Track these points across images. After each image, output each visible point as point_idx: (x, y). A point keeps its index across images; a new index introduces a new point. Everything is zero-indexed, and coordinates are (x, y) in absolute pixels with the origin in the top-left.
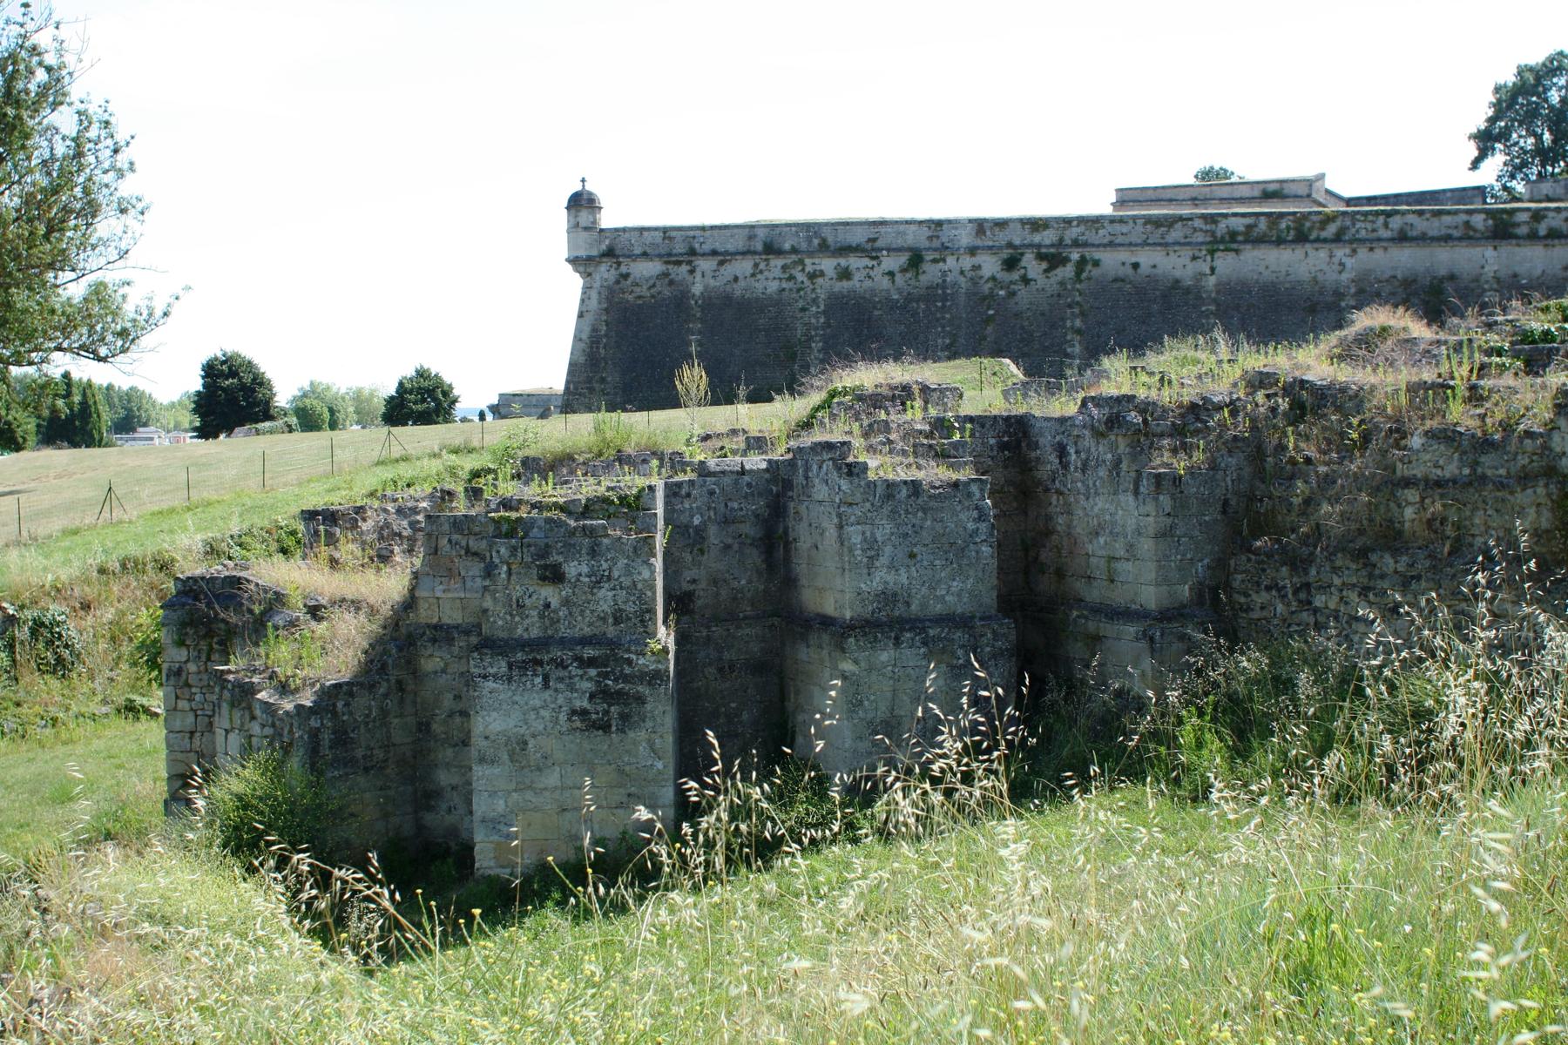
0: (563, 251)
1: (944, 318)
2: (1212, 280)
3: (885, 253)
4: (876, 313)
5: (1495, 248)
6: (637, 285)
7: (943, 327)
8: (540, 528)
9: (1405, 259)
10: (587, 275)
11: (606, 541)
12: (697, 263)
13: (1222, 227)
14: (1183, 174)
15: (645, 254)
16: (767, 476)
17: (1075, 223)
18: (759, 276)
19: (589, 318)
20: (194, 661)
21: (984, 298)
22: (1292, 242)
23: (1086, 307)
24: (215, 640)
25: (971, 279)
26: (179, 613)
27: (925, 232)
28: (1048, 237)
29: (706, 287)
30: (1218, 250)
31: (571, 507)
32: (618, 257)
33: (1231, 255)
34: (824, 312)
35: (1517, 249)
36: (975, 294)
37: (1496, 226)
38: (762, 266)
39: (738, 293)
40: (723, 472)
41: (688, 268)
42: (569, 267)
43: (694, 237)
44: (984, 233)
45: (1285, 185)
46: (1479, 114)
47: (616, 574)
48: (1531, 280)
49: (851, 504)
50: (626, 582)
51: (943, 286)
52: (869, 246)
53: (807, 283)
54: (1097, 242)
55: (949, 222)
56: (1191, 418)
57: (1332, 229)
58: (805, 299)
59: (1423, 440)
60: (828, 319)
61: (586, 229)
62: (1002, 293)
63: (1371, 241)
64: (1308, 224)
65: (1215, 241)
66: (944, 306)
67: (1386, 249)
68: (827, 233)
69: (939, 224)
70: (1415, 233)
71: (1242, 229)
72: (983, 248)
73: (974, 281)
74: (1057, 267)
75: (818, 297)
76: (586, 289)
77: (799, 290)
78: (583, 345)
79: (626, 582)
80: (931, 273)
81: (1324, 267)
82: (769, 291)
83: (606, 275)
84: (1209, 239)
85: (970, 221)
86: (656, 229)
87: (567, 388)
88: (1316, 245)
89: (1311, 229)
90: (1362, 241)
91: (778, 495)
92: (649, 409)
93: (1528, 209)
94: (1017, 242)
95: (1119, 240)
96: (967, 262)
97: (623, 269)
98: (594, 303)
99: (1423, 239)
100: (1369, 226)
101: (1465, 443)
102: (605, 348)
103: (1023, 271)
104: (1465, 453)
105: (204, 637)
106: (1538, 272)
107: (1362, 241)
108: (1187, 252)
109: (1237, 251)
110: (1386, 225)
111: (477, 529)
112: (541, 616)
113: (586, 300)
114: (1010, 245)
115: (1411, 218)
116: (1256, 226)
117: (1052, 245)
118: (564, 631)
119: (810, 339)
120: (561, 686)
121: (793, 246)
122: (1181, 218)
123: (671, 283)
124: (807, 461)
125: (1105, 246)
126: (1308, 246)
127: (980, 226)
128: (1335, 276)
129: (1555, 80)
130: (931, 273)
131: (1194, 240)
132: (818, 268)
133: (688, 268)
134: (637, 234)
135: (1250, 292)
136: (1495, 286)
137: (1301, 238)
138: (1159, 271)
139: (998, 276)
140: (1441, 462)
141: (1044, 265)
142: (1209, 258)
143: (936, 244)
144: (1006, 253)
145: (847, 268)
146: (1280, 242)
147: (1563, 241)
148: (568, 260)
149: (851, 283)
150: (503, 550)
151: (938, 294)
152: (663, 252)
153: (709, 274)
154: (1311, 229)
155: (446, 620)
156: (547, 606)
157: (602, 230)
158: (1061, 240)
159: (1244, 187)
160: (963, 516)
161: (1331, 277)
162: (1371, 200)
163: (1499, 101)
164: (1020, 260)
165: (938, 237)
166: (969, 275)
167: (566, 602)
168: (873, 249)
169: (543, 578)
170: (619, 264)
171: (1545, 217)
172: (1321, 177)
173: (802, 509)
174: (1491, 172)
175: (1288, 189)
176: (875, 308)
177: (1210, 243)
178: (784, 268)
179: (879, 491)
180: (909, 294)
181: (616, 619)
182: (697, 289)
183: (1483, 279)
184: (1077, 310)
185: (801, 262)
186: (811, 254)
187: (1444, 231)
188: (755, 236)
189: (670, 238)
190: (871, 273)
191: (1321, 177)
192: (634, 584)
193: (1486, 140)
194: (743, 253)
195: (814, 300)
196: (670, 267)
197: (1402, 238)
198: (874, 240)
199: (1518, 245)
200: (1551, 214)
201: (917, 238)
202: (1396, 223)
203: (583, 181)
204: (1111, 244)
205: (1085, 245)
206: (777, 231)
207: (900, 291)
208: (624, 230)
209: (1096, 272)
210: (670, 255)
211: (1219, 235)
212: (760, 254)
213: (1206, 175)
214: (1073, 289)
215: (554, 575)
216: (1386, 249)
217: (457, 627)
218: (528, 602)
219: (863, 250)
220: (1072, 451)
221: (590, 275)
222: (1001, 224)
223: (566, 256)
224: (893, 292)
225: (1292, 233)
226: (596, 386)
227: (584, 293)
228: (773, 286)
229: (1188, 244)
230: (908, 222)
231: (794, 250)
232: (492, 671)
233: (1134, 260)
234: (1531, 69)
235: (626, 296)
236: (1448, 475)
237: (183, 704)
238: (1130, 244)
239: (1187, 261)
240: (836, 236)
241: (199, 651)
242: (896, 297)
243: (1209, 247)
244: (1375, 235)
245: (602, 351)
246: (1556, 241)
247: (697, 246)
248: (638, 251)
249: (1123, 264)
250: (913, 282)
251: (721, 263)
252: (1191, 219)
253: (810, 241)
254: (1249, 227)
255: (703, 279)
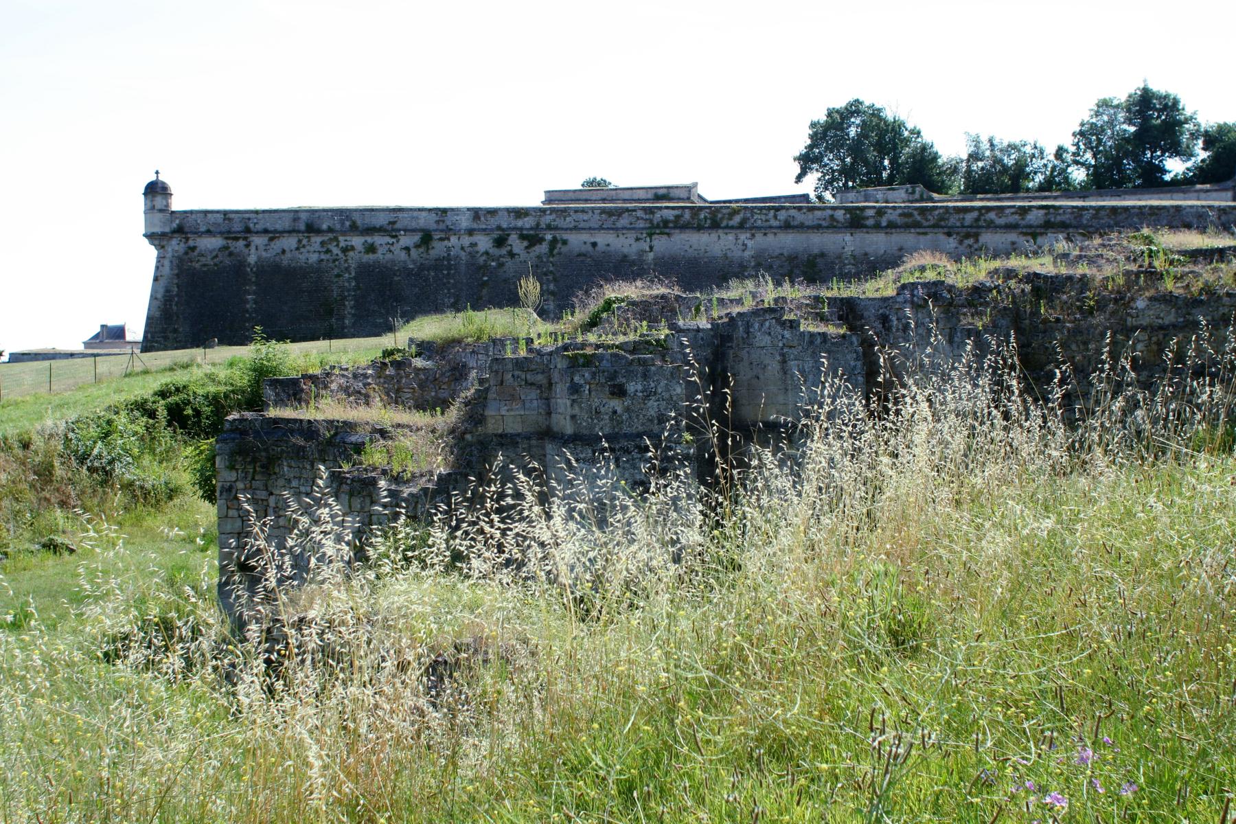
0: (142, 230)
1: (449, 283)
2: (651, 255)
3: (402, 232)
4: (396, 278)
5: (852, 234)
6: (203, 255)
7: (449, 290)
8: (607, 360)
9: (788, 242)
10: (160, 247)
11: (653, 368)
12: (251, 239)
13: (658, 216)
14: (575, 184)
15: (208, 232)
16: (712, 333)
17: (548, 212)
18: (302, 250)
19: (162, 282)
20: (242, 481)
21: (480, 268)
22: (709, 228)
23: (558, 275)
24: (258, 464)
25: (470, 253)
26: (231, 445)
27: (434, 217)
28: (528, 222)
29: (259, 258)
30: (655, 233)
31: (625, 347)
32: (187, 233)
33: (665, 237)
34: (355, 278)
35: (867, 236)
36: (472, 265)
37: (852, 218)
38: (305, 242)
39: (285, 263)
40: (688, 330)
41: (245, 243)
42: (146, 241)
43: (249, 219)
44: (479, 218)
45: (671, 190)
46: (801, 142)
47: (660, 390)
48: (877, 258)
49: (791, 347)
50: (666, 395)
51: (448, 258)
52: (389, 228)
53: (341, 255)
54: (565, 227)
55: (452, 210)
56: (976, 296)
57: (737, 219)
58: (339, 268)
59: (1147, 302)
60: (358, 283)
61: (161, 211)
62: (493, 264)
63: (765, 228)
64: (720, 216)
65: (653, 227)
66: (448, 274)
67: (775, 234)
68: (356, 217)
69: (444, 211)
70: (796, 223)
71: (672, 218)
72: (479, 230)
73: (472, 255)
74: (535, 245)
75: (349, 266)
76: (160, 259)
77: (334, 261)
78: (158, 303)
79: (666, 395)
80: (438, 248)
81: (732, 247)
82: (310, 261)
83: (176, 248)
84: (648, 225)
85: (469, 209)
86: (218, 212)
87: (145, 337)
88: (726, 231)
89: (722, 219)
90: (759, 228)
91: (718, 346)
92: (330, 338)
93: (874, 207)
94: (505, 226)
95: (582, 225)
96: (466, 241)
97: (191, 243)
98: (166, 270)
99: (801, 227)
100: (763, 217)
101: (1180, 302)
102: (176, 305)
103: (509, 248)
104: (1179, 308)
105: (250, 463)
106: (882, 252)
107: (759, 228)
108: (632, 235)
109: (668, 234)
110: (775, 217)
111: (533, 367)
112: (611, 419)
113: (161, 268)
114: (499, 228)
115: (793, 212)
116: (682, 216)
117: (531, 229)
118: (626, 429)
119: (344, 298)
120: (627, 465)
121: (329, 227)
122: (627, 210)
123: (231, 254)
124: (748, 322)
125: (571, 229)
126: (720, 231)
127: (476, 213)
128: (740, 253)
129: (853, 120)
130: (438, 248)
131: (637, 226)
132: (349, 244)
133: (245, 243)
134: (202, 215)
135: (679, 265)
136: (852, 261)
137: (715, 225)
138: (612, 248)
139: (491, 251)
140: (1162, 315)
141: (526, 243)
142: (648, 239)
143: (442, 226)
144: (496, 234)
145: (373, 244)
146: (699, 228)
147: (898, 230)
148: (146, 235)
149: (376, 255)
150: (587, 375)
151: (444, 264)
152: (223, 230)
153: (261, 248)
154: (722, 219)
155: (509, 431)
156: (615, 412)
157: (173, 212)
158: (538, 224)
159: (641, 191)
160: (848, 357)
161: (737, 254)
162: (746, 201)
163: (815, 134)
164: (507, 239)
165: (443, 221)
166: (468, 250)
167: (627, 410)
168: (393, 230)
169: (613, 394)
170: (187, 239)
171: (886, 213)
172: (695, 185)
173: (744, 354)
174: (810, 185)
175: (674, 193)
176: (395, 275)
177: (649, 228)
178: (322, 243)
179: (806, 338)
180: (422, 264)
181: (659, 420)
182: (252, 259)
183: (844, 256)
184: (551, 277)
185: (336, 239)
186: (344, 233)
187: (816, 222)
188: (299, 218)
189: (229, 219)
190: (392, 248)
191: (695, 185)
192: (671, 397)
193: (807, 161)
194: (289, 232)
195: (347, 269)
196: (229, 242)
197: (787, 226)
198: (394, 223)
199: (868, 233)
200: (890, 211)
201: (429, 222)
202: (782, 215)
203: (157, 173)
204: (575, 228)
205: (556, 228)
206: (317, 215)
207: (414, 262)
208: (191, 212)
209: (564, 249)
210: (229, 232)
211: (655, 223)
212: (303, 232)
213: (591, 183)
214: (548, 261)
215: (619, 392)
216: (775, 234)
217: (519, 435)
218: (603, 410)
219: (385, 231)
220: (894, 319)
221: (163, 247)
222: (492, 212)
223: (143, 232)
224: (409, 262)
225: (709, 221)
226: (170, 335)
227: (158, 261)
228: (314, 258)
229: (634, 229)
230: (420, 210)
231: (330, 230)
232: (582, 456)
233: (593, 240)
234: (837, 111)
235: (193, 264)
236: (1167, 322)
237: (232, 513)
238: (590, 228)
239: (632, 241)
240: (363, 219)
241: (246, 473)
242: (411, 266)
243: (648, 231)
244: (768, 224)
245: (175, 308)
246: (894, 230)
247: (251, 225)
248: (203, 229)
249: (585, 243)
250: (424, 255)
251: (271, 239)
252: (635, 211)
253: (343, 224)
254: (678, 217)
255: (257, 252)
